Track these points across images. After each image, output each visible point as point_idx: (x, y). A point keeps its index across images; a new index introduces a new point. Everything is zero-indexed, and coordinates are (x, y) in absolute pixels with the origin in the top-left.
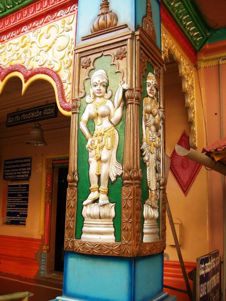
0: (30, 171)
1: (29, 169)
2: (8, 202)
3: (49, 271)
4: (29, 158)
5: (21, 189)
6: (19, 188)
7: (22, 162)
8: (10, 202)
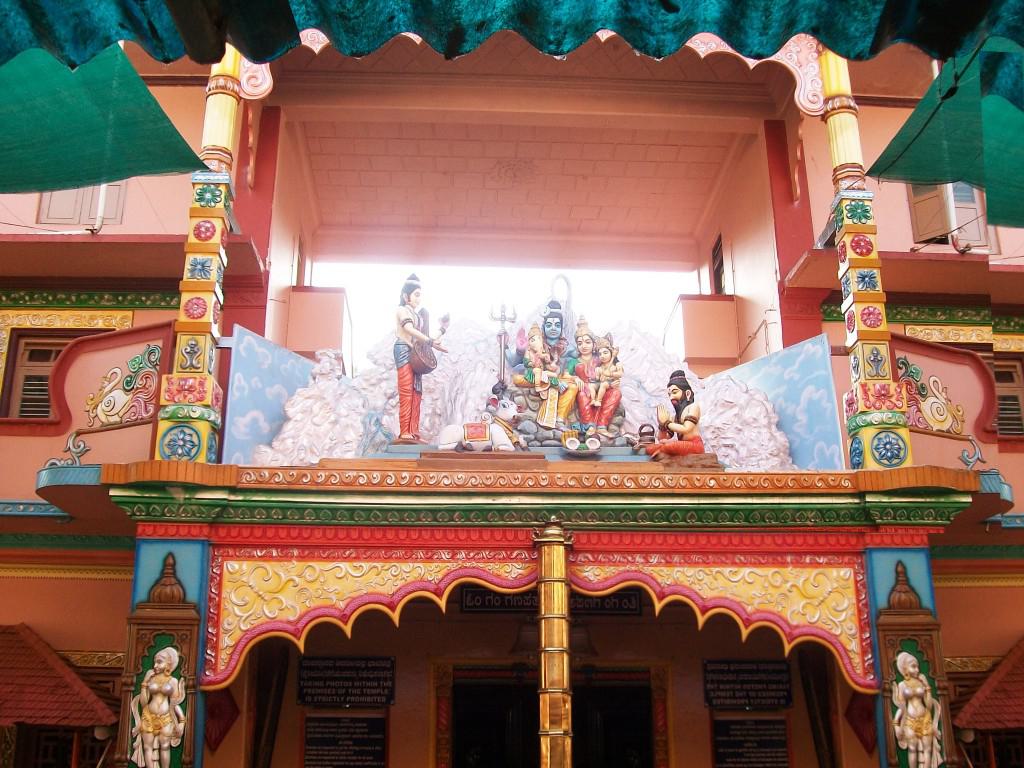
0: (392, 690)
1: (389, 684)
2: (307, 757)
3: (847, 468)
4: (388, 659)
5: (348, 727)
6: (341, 725)
7: (363, 666)
8: (314, 758)
